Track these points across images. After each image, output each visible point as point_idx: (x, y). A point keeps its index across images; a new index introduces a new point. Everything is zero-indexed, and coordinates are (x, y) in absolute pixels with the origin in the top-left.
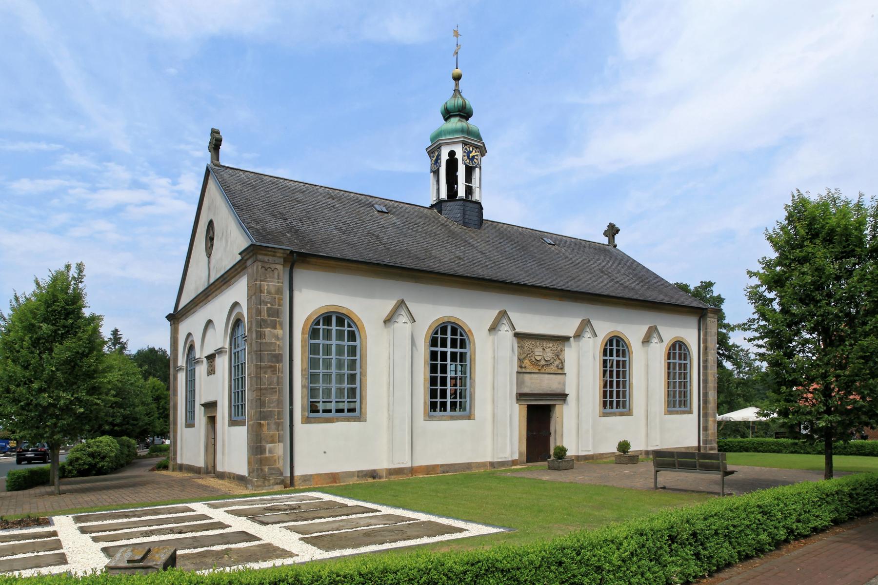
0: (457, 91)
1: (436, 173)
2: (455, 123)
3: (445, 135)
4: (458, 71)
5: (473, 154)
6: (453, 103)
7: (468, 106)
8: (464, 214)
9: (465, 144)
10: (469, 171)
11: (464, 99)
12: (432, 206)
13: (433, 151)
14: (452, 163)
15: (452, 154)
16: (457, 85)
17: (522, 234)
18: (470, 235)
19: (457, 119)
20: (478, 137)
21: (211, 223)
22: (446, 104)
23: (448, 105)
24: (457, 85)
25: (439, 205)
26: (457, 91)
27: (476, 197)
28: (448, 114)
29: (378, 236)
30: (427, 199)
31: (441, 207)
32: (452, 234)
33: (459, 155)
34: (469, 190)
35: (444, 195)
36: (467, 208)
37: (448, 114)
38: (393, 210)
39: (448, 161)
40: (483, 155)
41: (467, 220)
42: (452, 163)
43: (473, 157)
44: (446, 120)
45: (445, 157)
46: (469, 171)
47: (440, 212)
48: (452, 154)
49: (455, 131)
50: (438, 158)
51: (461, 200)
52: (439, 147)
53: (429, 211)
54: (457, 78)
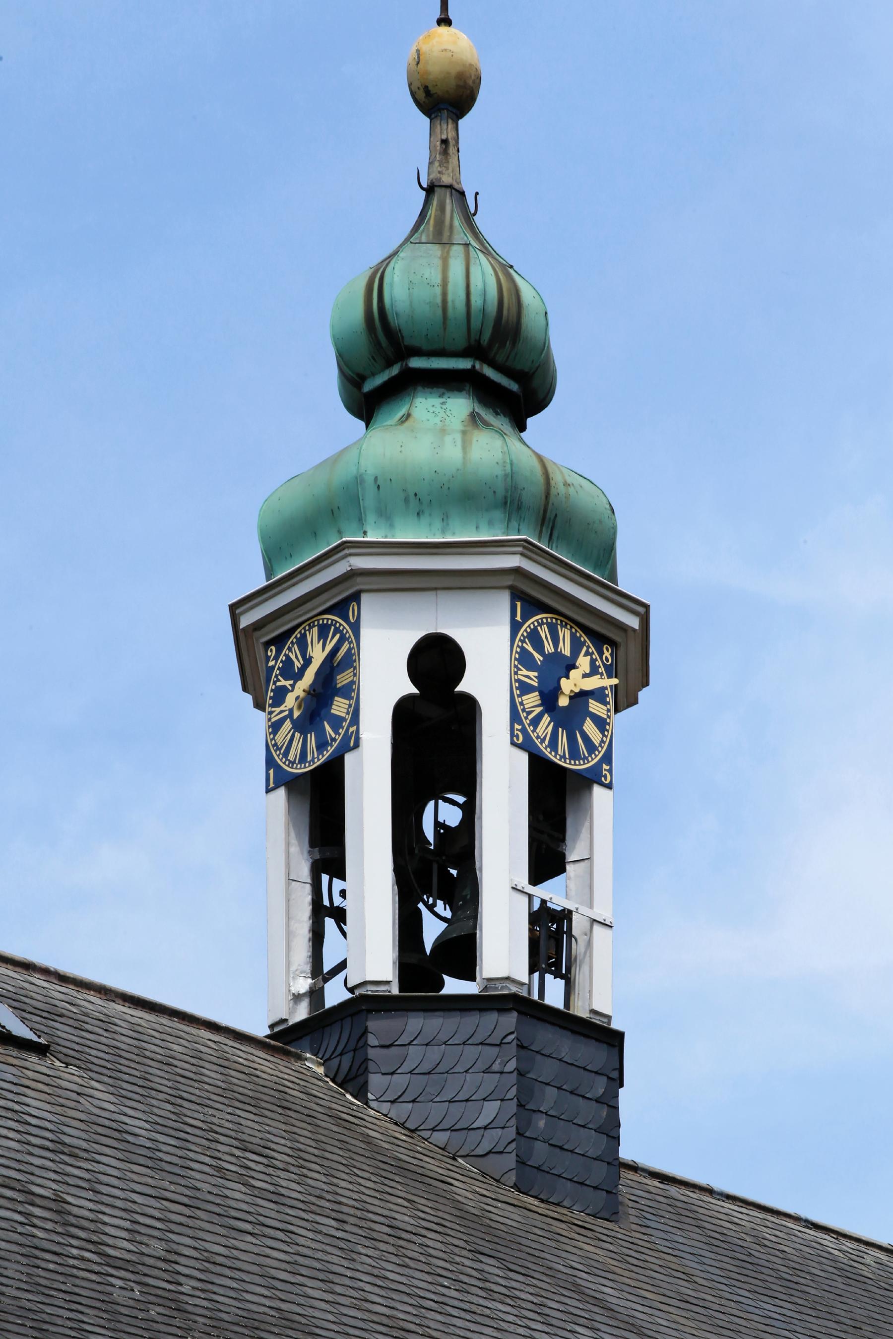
0: (444, 202)
1: (320, 802)
2: (437, 433)
3: (385, 515)
4: (453, 45)
5: (571, 684)
6: (420, 284)
7: (531, 319)
8: (524, 1108)
9: (528, 598)
10: (555, 797)
11: (505, 269)
12: (286, 1039)
13: (284, 640)
14: (436, 738)
15: (436, 661)
16: (445, 148)
17: (850, 1275)
18: (586, 1251)
19: (459, 406)
20: (597, 547)
21: (323, 650)
22: (376, 282)
23: (399, 291)
24: (445, 148)
25: (333, 1032)
26: (444, 202)
27: (604, 987)
28: (385, 365)
29: (58, 1206)
30: (248, 981)
31: (360, 1043)
32: (485, 1238)
33: (489, 674)
34: (550, 938)
35: (371, 953)
36: (545, 1070)
37: (385, 365)
38: (63, 1032)
39: (404, 714)
40: (625, 699)
41: (540, 1153)
42: (436, 738)
43: (582, 697)
44: (366, 404)
45: (383, 679)
46: (555, 797)
47: (353, 1080)
48: (436, 661)
49: (460, 495)
50: (334, 683)
51: (500, 1001)
52: (341, 603)
53: (268, 1066)
54: (446, 99)
